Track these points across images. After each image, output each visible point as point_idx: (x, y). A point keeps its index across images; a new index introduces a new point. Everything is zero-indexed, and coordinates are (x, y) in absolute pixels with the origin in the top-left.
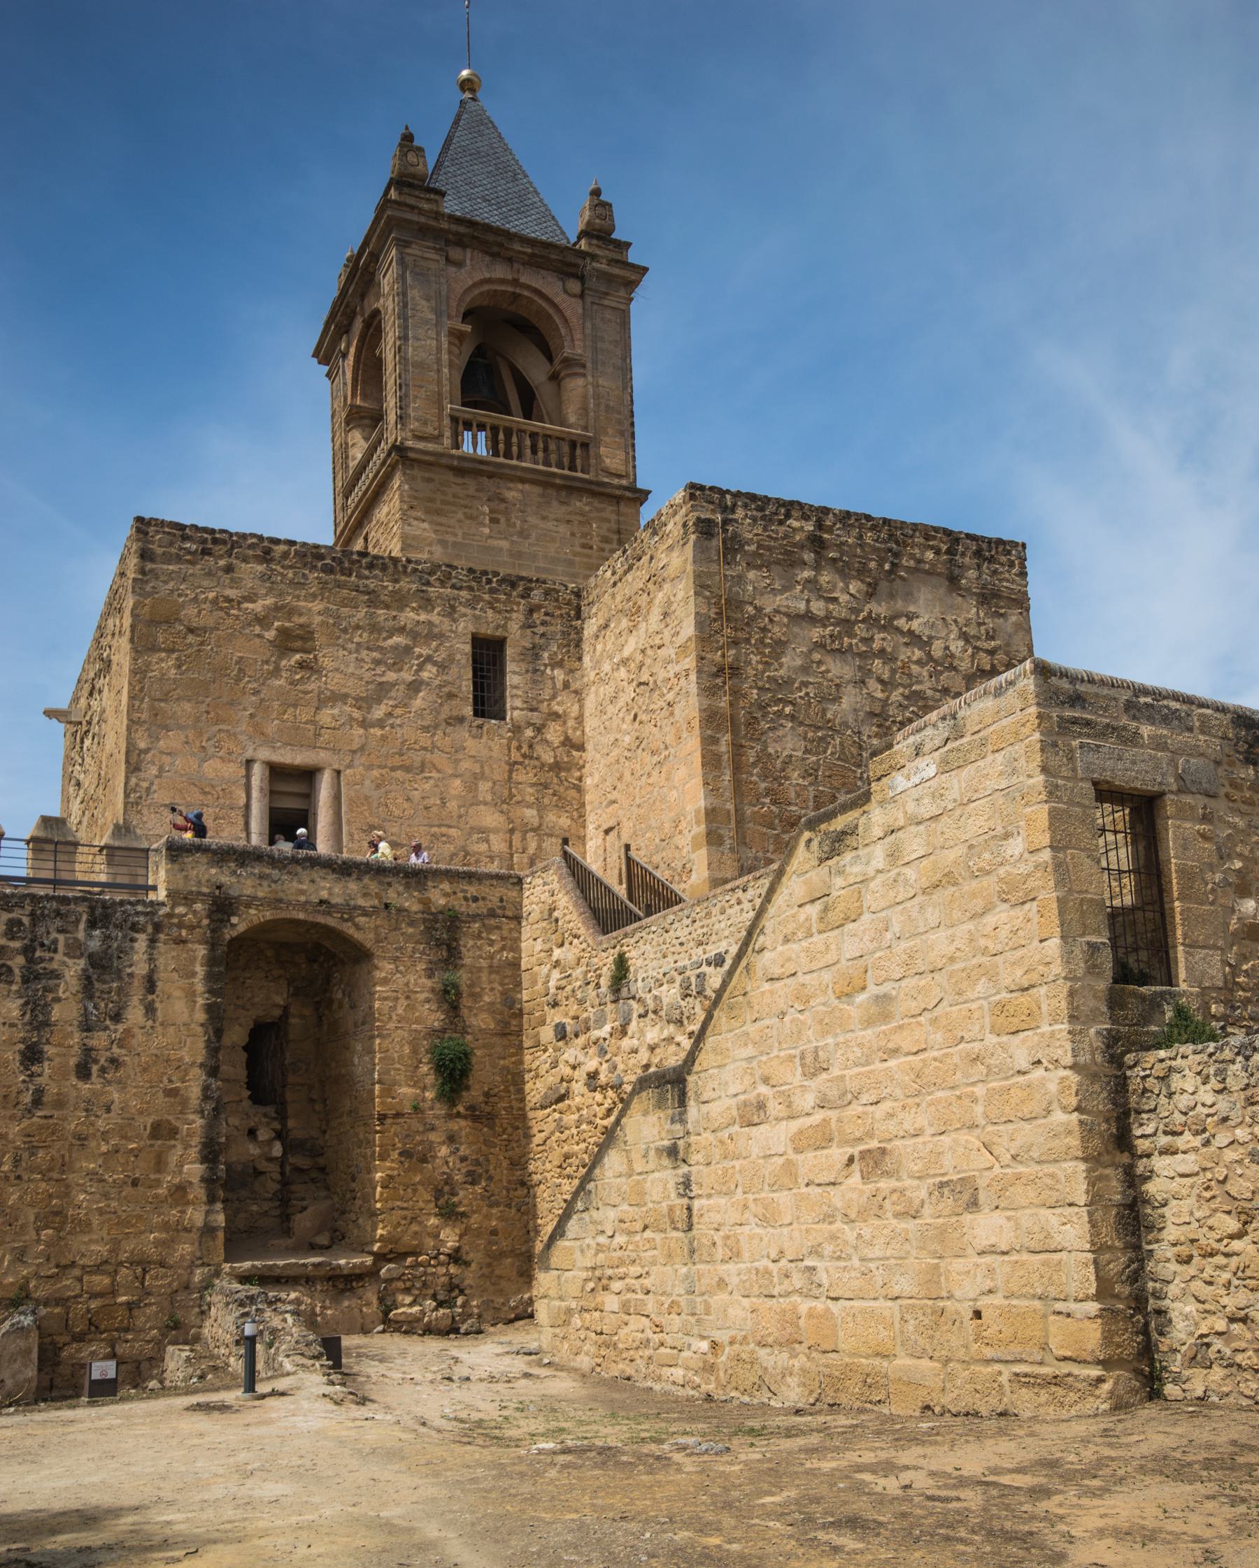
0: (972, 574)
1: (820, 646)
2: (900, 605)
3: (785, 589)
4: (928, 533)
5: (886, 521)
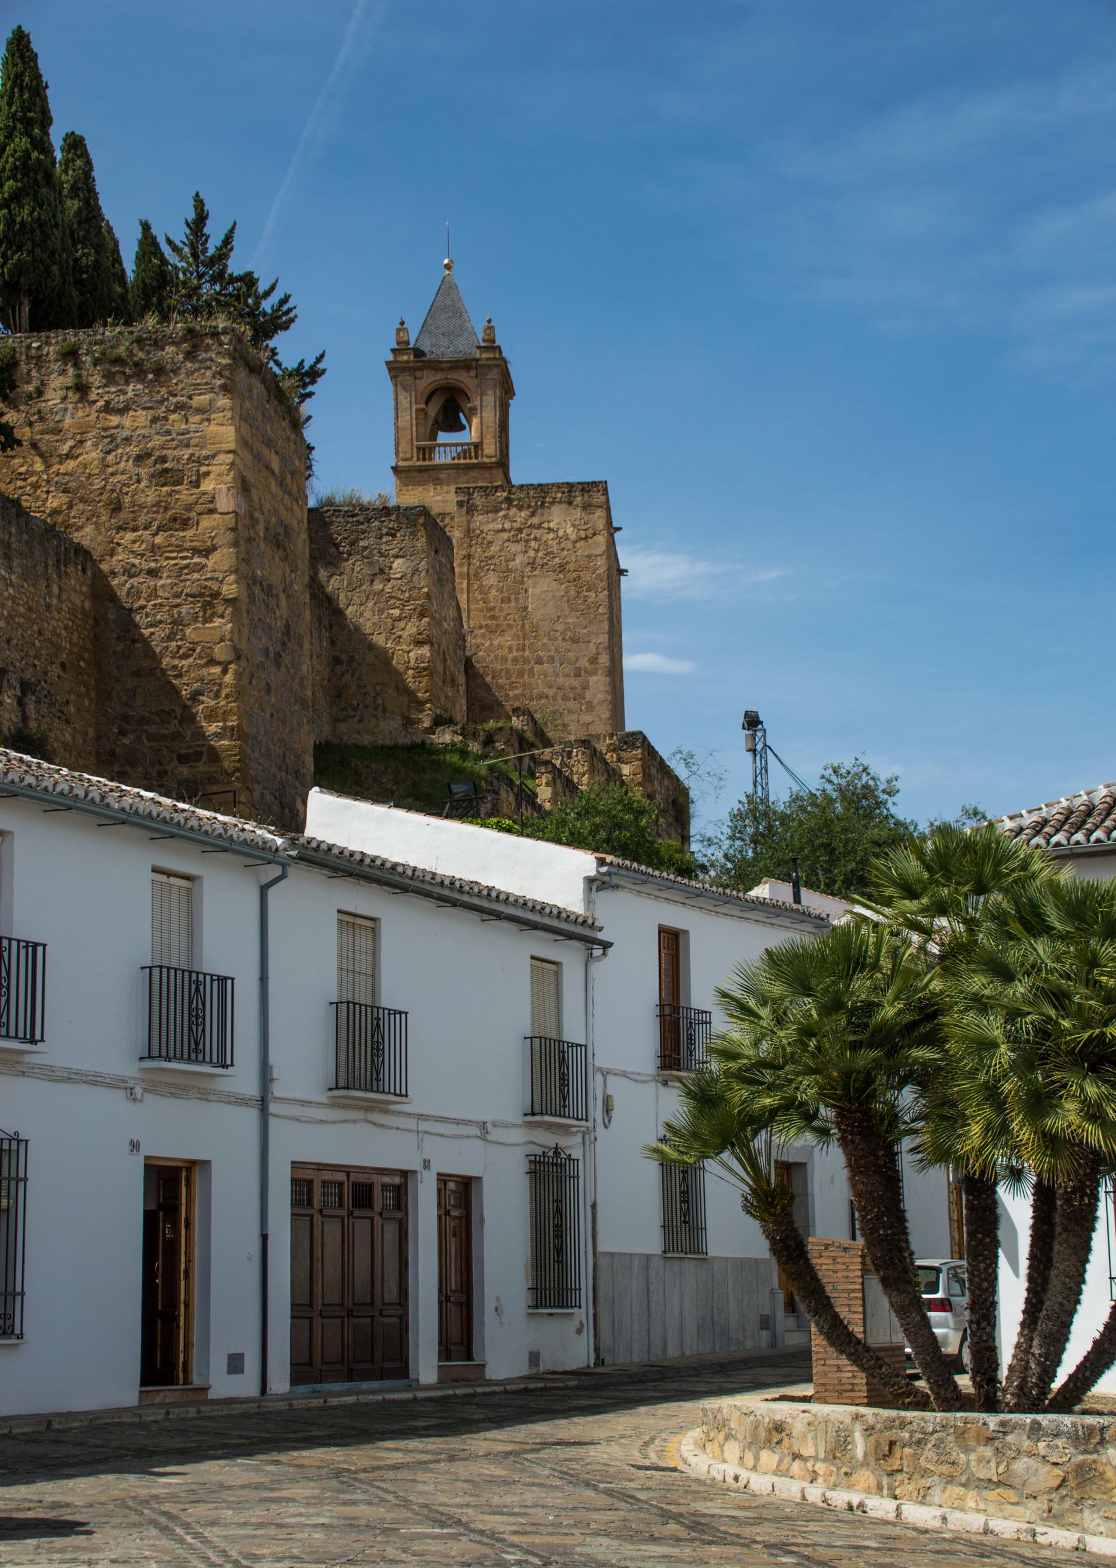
0: (579, 499)
1: (508, 540)
2: (545, 518)
3: (493, 521)
4: (559, 486)
5: (540, 485)
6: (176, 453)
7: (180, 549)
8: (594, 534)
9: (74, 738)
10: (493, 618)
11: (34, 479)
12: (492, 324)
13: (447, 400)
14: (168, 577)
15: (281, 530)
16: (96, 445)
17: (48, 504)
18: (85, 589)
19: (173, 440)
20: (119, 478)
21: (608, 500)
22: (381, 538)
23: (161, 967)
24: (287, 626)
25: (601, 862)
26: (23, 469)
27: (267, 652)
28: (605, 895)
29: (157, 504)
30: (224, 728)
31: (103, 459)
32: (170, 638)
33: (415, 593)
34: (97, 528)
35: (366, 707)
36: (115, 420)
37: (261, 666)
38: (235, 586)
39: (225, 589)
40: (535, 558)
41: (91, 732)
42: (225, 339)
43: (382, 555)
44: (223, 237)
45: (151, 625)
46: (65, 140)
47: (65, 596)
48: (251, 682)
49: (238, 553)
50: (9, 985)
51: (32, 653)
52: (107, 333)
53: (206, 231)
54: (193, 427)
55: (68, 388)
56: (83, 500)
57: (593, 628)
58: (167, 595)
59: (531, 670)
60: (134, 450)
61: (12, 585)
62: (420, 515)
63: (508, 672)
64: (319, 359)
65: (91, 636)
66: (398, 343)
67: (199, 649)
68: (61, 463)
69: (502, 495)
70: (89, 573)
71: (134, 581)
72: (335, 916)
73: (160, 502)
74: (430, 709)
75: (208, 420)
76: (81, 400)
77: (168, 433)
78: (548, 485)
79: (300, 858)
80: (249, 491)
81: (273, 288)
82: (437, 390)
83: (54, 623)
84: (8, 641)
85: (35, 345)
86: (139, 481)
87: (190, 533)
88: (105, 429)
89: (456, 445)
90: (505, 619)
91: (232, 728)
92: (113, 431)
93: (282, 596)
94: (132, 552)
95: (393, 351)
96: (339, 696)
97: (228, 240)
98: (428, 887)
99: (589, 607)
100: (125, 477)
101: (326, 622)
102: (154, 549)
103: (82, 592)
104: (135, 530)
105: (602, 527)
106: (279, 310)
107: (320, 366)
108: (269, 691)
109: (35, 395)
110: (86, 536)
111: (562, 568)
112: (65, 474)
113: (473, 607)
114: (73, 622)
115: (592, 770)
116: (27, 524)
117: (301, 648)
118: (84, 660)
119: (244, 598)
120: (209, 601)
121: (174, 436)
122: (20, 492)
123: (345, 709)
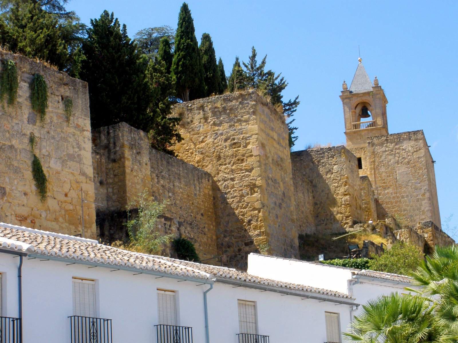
1: (388, 155)
4: (405, 133)
6: (238, 136)
7: (241, 170)
8: (420, 149)
9: (208, 240)
10: (384, 183)
11: (191, 151)
12: (377, 79)
13: (363, 107)
14: (238, 180)
15: (279, 160)
16: (211, 137)
17: (196, 159)
18: (209, 187)
19: (237, 132)
20: (219, 147)
21: (424, 136)
22: (328, 159)
23: (160, 325)
24: (284, 194)
25: (354, 274)
26: (187, 148)
27: (275, 204)
28: (357, 286)
29: (233, 155)
30: (260, 232)
31: (214, 141)
32: (239, 202)
33: (342, 177)
34: (213, 166)
35: (327, 220)
36: (217, 128)
37: (274, 208)
38: (261, 181)
39: (257, 183)
40: (398, 160)
41: (214, 237)
42: (253, 96)
43: (329, 165)
44: (262, 61)
45: (232, 198)
46: (202, 36)
47: (201, 190)
48: (269, 215)
49: (261, 169)
50: (97, 335)
51: (190, 211)
52: (213, 98)
53: (256, 59)
54: (243, 127)
55: (201, 119)
56: (207, 156)
57: (422, 184)
58: (237, 186)
59: (400, 201)
60: (224, 137)
61: (181, 188)
62: (342, 149)
63: (391, 202)
64: (297, 98)
65: (213, 203)
66: (344, 89)
67: (249, 205)
68: (199, 144)
69: (384, 138)
70: (211, 181)
71: (226, 183)
72: (237, 302)
73: (233, 154)
74: (351, 219)
75: (249, 124)
76: (206, 122)
77: (235, 130)
78: (401, 133)
79: (218, 281)
80: (264, 147)
81: (278, 76)
82: (359, 104)
83: (198, 200)
84: (181, 208)
85: (190, 105)
86: (226, 148)
87: (244, 164)
88: (214, 131)
89: (367, 122)
90: (389, 183)
91: (263, 232)
92: (216, 132)
93: (281, 183)
94: (225, 173)
95: (342, 92)
96: (317, 217)
97: (264, 63)
98: (276, 289)
99: (420, 176)
100: (221, 147)
101: (311, 190)
102: (232, 171)
103: (208, 188)
104: (225, 165)
105: (422, 146)
106: (281, 83)
107: (297, 101)
108: (277, 217)
109: (190, 122)
110: (209, 169)
111: (408, 163)
112: (201, 148)
113: (377, 180)
114: (205, 199)
115: (410, 236)
116: (186, 167)
117: (290, 200)
118: (210, 212)
119: (265, 186)
120: (252, 187)
121: (237, 130)
122: (187, 156)
123: (320, 221)
